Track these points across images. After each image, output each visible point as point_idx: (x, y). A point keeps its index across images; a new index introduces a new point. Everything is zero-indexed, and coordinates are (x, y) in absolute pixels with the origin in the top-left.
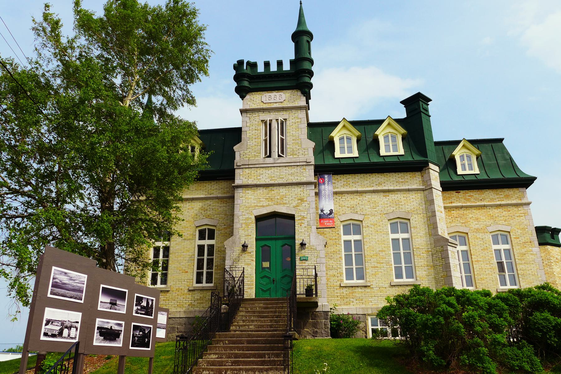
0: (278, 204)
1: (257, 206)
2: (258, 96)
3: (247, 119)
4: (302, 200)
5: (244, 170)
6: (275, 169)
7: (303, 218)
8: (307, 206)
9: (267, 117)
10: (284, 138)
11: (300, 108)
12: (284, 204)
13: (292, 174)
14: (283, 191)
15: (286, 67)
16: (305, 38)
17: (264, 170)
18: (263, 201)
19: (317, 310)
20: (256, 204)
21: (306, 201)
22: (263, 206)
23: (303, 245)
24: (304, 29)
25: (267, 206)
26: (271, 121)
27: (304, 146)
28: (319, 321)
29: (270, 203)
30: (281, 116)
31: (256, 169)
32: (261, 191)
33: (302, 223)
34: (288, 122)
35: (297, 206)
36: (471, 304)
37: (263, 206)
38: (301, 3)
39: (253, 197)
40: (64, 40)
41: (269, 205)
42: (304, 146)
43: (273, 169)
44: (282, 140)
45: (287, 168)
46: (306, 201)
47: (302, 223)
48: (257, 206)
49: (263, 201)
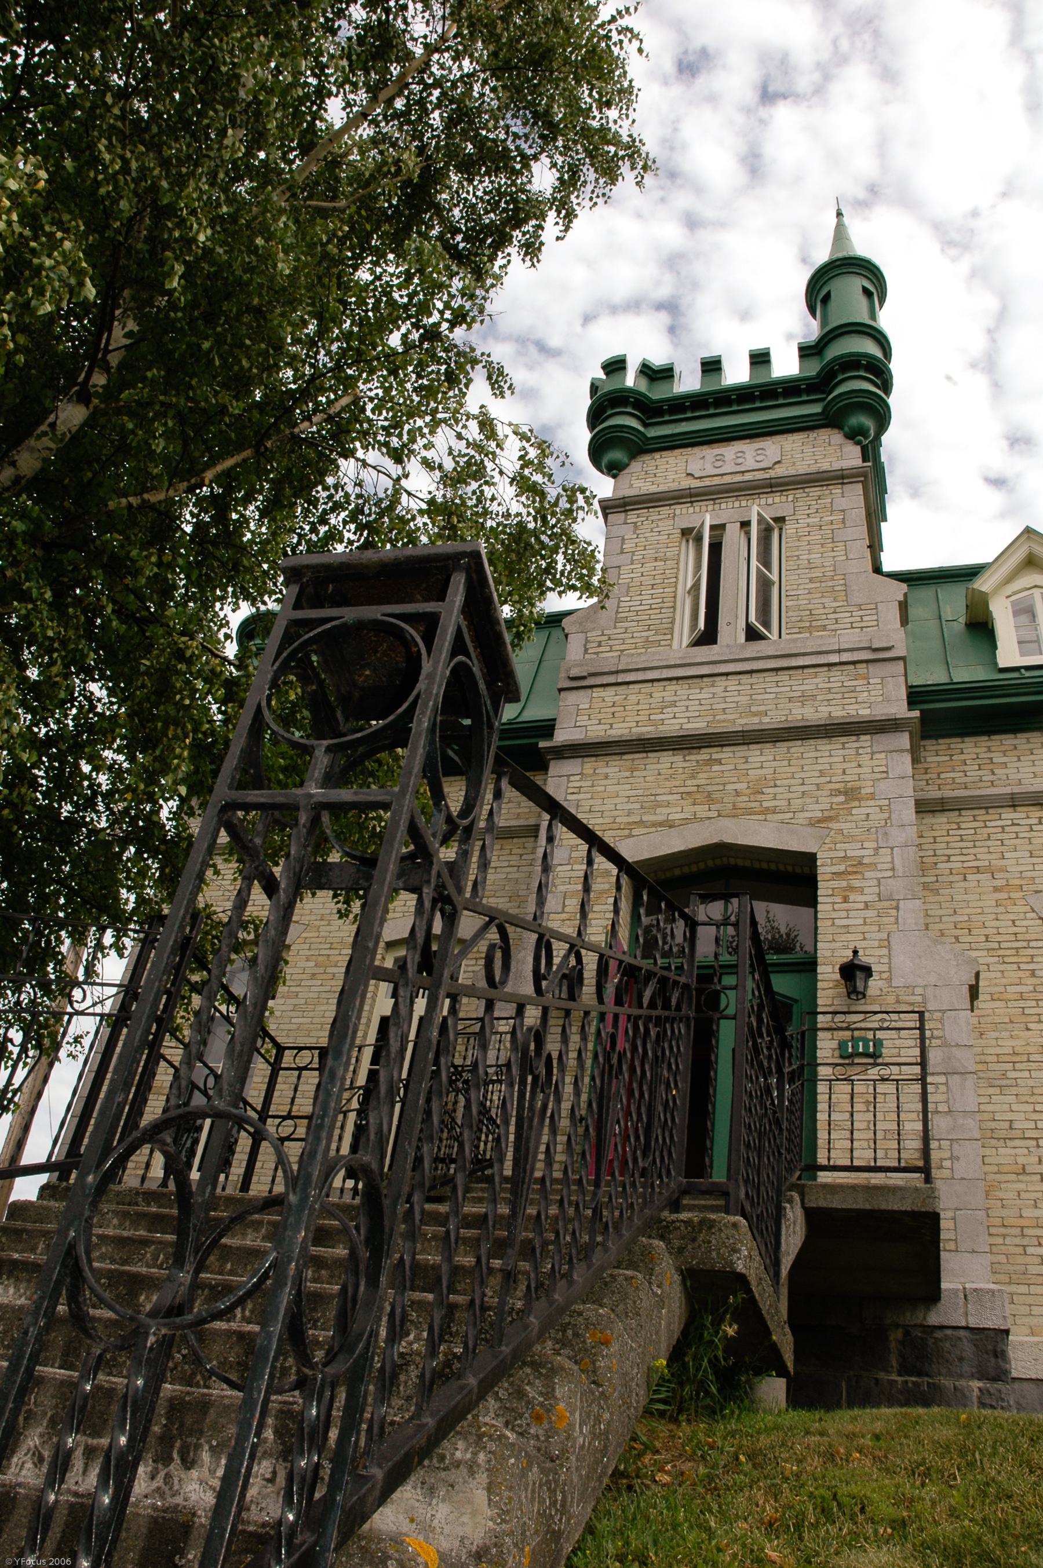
0: (735, 813)
1: (641, 823)
2: (672, 460)
3: (627, 531)
4: (851, 794)
5: (597, 693)
6: (732, 683)
7: (858, 866)
8: (877, 817)
9: (706, 517)
10: (774, 577)
11: (841, 478)
12: (766, 811)
13: (804, 698)
14: (761, 760)
15: (786, 365)
16: (854, 285)
17: (682, 690)
18: (668, 804)
19: (934, 1318)
20: (636, 818)
21: (872, 796)
22: (670, 825)
23: (854, 973)
24: (851, 254)
25: (686, 821)
26: (718, 529)
27: (857, 598)
28: (947, 1383)
29: (702, 810)
30: (755, 510)
31: (647, 688)
32: (666, 760)
33: (851, 888)
34: (789, 529)
35: (830, 819)
36: (81, 1037)
37: (670, 825)
38: (839, 214)
39: (625, 790)
40: (58, 433)
41: (695, 819)
42: (857, 598)
43: (721, 682)
44: (765, 585)
45: (783, 676)
46: (872, 796)
47: (851, 888)
48: (641, 823)
49: (668, 804)
